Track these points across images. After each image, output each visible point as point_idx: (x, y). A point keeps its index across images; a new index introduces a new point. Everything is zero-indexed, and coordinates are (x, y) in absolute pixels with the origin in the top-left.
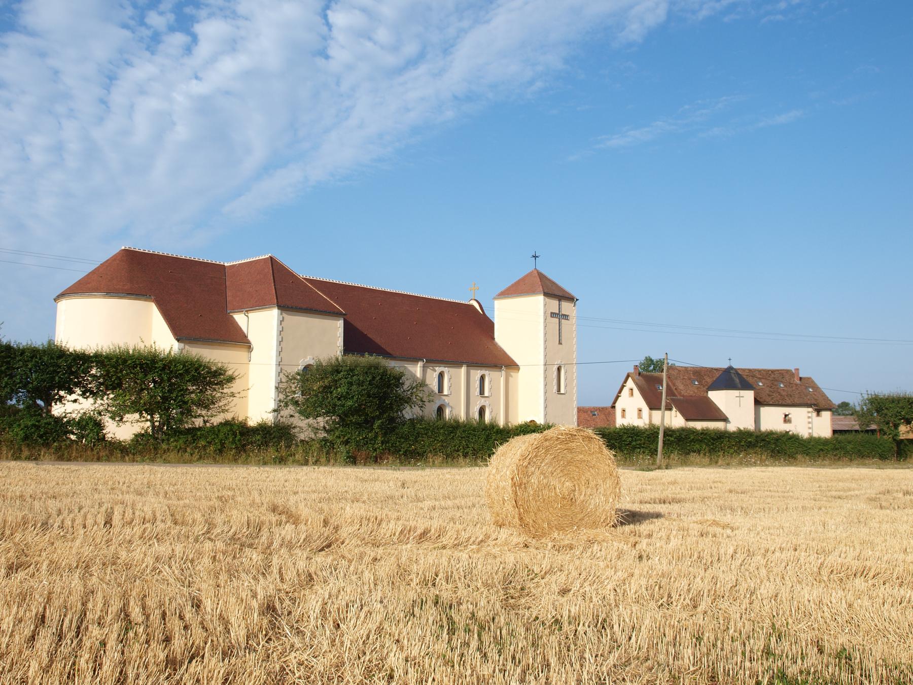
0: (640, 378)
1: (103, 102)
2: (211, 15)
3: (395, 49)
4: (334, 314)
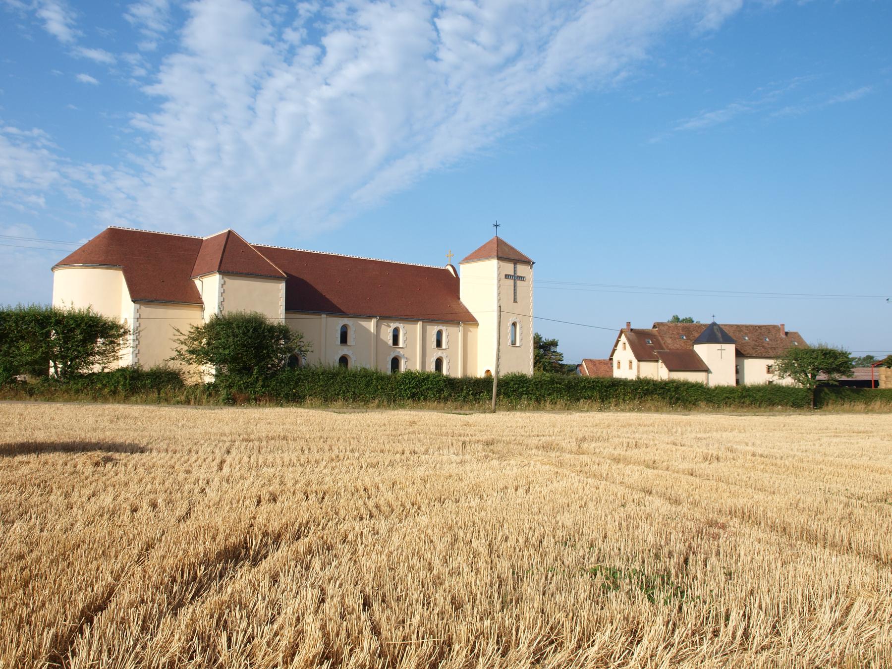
0: (632, 334)
1: (251, 108)
2: (337, 28)
3: (496, 49)
4: (276, 277)
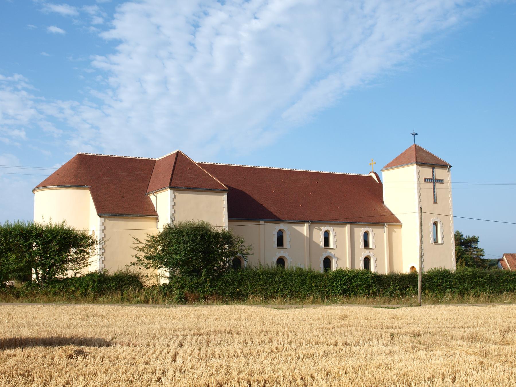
1: (192, 44)
4: (218, 190)
